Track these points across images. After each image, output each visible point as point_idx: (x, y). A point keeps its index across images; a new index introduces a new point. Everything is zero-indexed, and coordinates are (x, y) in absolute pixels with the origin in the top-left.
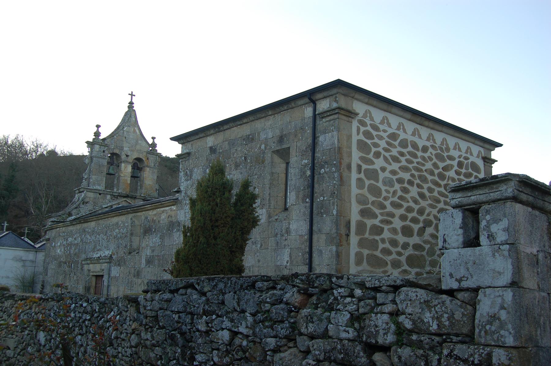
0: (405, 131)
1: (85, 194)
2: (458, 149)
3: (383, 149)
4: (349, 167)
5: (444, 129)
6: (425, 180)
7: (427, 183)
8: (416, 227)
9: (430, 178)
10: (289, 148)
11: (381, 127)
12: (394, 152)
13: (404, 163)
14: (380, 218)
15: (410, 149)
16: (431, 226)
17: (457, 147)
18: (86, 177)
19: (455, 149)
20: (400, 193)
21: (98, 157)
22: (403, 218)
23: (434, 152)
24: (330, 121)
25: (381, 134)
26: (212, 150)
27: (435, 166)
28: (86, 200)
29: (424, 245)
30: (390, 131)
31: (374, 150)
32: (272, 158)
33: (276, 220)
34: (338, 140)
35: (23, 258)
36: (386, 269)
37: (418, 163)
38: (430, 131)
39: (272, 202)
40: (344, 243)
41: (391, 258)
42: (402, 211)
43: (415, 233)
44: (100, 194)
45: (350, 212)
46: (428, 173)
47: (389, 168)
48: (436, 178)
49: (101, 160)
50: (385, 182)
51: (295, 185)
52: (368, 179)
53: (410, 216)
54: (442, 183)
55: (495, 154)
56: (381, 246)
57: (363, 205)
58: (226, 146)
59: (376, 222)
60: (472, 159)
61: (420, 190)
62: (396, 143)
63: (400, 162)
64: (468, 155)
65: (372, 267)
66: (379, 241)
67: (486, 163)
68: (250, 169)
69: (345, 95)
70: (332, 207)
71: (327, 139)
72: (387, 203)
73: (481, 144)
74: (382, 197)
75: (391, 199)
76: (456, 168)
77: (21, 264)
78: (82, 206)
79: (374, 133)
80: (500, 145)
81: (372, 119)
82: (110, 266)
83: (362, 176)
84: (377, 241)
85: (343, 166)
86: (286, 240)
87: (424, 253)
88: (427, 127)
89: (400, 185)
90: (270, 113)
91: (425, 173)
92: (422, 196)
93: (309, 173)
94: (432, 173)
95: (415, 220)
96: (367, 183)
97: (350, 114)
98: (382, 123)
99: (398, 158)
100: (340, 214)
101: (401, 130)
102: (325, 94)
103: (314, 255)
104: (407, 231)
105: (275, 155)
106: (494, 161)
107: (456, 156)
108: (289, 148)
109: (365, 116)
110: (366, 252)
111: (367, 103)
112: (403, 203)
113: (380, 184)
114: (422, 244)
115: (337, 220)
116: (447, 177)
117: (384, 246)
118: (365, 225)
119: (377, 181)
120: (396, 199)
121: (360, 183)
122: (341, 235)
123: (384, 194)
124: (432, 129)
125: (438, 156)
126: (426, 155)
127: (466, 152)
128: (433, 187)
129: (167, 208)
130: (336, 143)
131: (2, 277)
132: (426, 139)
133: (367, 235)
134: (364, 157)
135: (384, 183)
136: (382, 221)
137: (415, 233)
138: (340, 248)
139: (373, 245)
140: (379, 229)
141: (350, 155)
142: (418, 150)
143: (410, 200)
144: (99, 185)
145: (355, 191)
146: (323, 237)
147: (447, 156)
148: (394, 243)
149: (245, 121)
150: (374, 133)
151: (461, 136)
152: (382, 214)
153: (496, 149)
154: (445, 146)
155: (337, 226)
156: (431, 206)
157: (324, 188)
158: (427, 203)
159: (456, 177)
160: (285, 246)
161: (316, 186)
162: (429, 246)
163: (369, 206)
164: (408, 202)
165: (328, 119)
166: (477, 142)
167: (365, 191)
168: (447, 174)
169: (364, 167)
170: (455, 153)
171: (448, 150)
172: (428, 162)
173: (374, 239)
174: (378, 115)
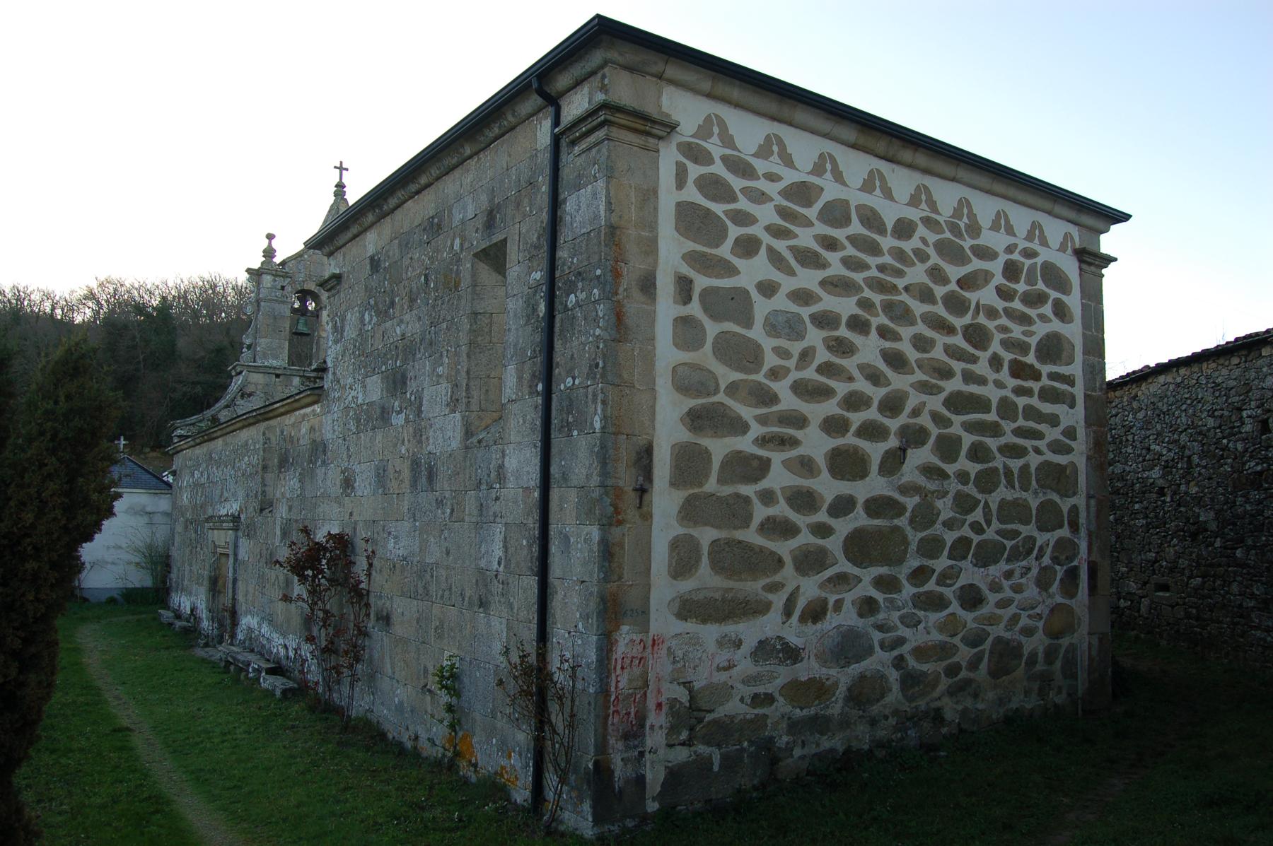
0: (838, 177)
1: (246, 379)
2: (1003, 228)
3: (768, 229)
4: (648, 285)
5: (962, 173)
6: (905, 316)
7: (913, 323)
8: (875, 451)
9: (918, 308)
10: (505, 240)
11: (760, 166)
12: (805, 238)
13: (836, 268)
14: (756, 430)
15: (856, 227)
16: (923, 443)
17: (1001, 223)
18: (248, 342)
19: (995, 227)
20: (823, 356)
21: (270, 301)
22: (834, 426)
23: (932, 238)
24: (589, 149)
25: (762, 185)
26: (375, 263)
27: (937, 275)
28: (248, 390)
29: (901, 499)
30: (790, 177)
31: (734, 232)
32: (474, 275)
33: (480, 442)
34: (609, 203)
35: (149, 509)
36: (777, 578)
37: (881, 268)
38: (918, 178)
39: (475, 393)
40: (631, 514)
41: (794, 543)
42: (831, 407)
43: (874, 467)
44: (278, 376)
45: (653, 420)
46: (914, 297)
47: (788, 284)
48: (940, 310)
49: (277, 306)
50: (773, 326)
51: (515, 345)
52: (715, 317)
53: (857, 418)
54: (958, 322)
55: (1109, 242)
56: (760, 512)
57: (697, 397)
58: (395, 251)
59: (745, 444)
60: (1044, 255)
61: (888, 345)
62: (812, 213)
63: (823, 265)
64: (1035, 245)
65: (730, 577)
66: (755, 500)
67: (1084, 266)
68: (433, 307)
69: (631, 69)
70: (592, 409)
71: (583, 206)
72: (782, 388)
73: (1072, 215)
74: (766, 368)
75: (794, 375)
76: (999, 279)
77: (143, 521)
78: (239, 401)
79: (737, 183)
80: (1123, 217)
81: (728, 141)
82: (237, 538)
83: (695, 309)
84: (747, 500)
85: (624, 283)
86: (497, 499)
87: (902, 522)
88: (911, 166)
89: (824, 334)
90: (468, 151)
91: (904, 297)
92: (896, 361)
93: (542, 308)
94: (926, 296)
95: (872, 431)
96: (712, 329)
97: (654, 128)
98: (763, 152)
99: (816, 254)
100: (613, 428)
101: (828, 175)
102: (577, 70)
103: (553, 549)
104: (847, 464)
105: (482, 265)
106: (1108, 260)
107: (1000, 248)
108: (505, 240)
109: (704, 131)
110: (707, 536)
111: (710, 96)
112: (832, 383)
113: (757, 333)
114: (897, 496)
115: (603, 447)
116: (973, 306)
117: (771, 511)
118: (705, 455)
119: (748, 323)
120: (810, 373)
121: (687, 331)
122: (618, 492)
123: (770, 360)
124: (927, 171)
125: (947, 250)
126: (908, 246)
127: (1030, 237)
128: (929, 333)
129: (308, 410)
130: (602, 213)
131: (108, 548)
132: (906, 199)
133: (711, 485)
134: (704, 255)
135: (772, 328)
136: (763, 441)
137: (874, 467)
138: (616, 532)
139: (737, 511)
140: (755, 463)
141: (651, 247)
142: (882, 231)
143: (856, 373)
144: (276, 357)
145: (667, 353)
146: (573, 496)
147: (972, 248)
148: (804, 500)
149: (423, 180)
150: (737, 183)
151: (1011, 192)
152: (763, 420)
153: (1113, 227)
154: (965, 219)
155: (604, 464)
156: (924, 388)
157: (577, 347)
158: (912, 379)
159: (1000, 304)
160: (495, 516)
161: (558, 344)
162: (917, 499)
163: (721, 397)
164: (851, 379)
165: (584, 145)
166: (1059, 209)
167: (706, 356)
168: (972, 297)
169: (702, 282)
170: (997, 241)
171: (974, 230)
172: (913, 264)
173: (737, 495)
174: (748, 131)
